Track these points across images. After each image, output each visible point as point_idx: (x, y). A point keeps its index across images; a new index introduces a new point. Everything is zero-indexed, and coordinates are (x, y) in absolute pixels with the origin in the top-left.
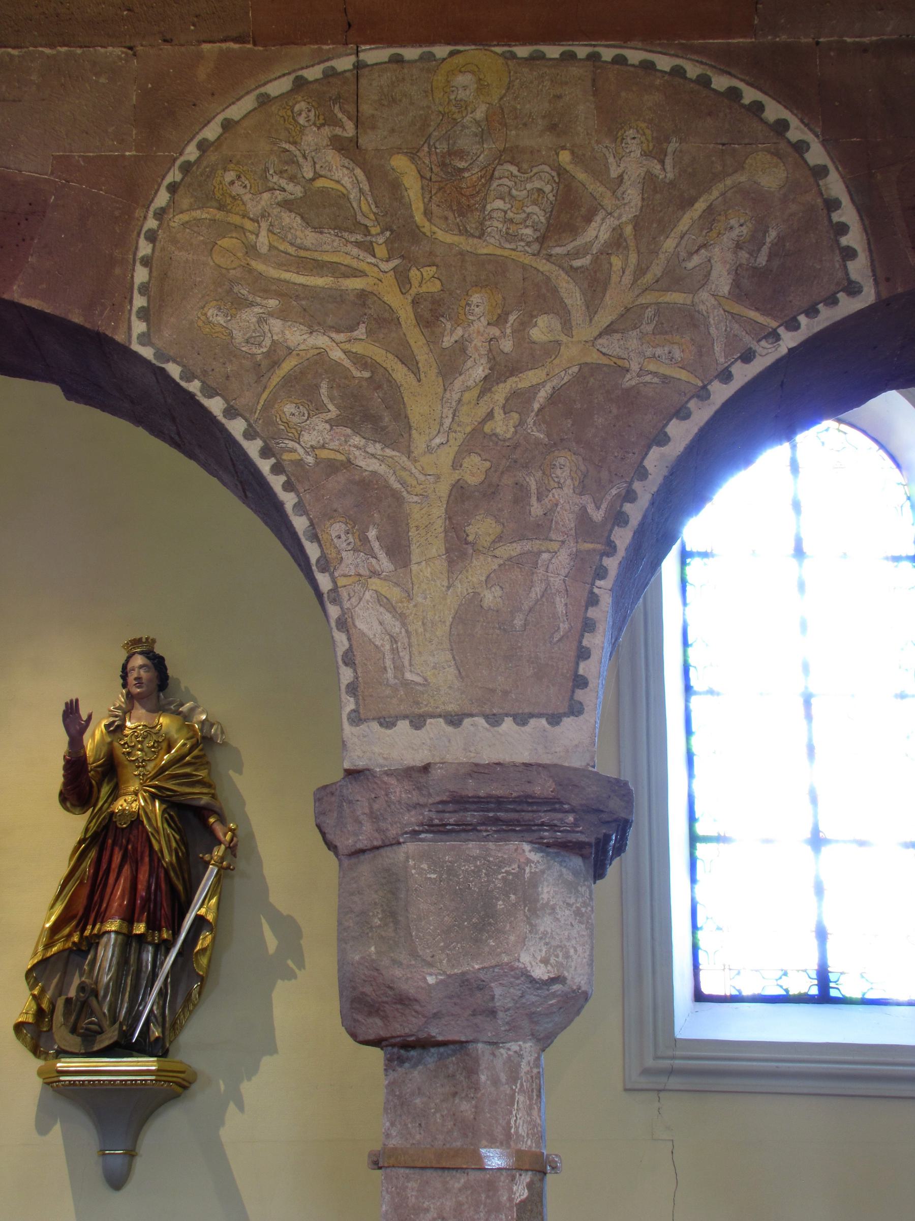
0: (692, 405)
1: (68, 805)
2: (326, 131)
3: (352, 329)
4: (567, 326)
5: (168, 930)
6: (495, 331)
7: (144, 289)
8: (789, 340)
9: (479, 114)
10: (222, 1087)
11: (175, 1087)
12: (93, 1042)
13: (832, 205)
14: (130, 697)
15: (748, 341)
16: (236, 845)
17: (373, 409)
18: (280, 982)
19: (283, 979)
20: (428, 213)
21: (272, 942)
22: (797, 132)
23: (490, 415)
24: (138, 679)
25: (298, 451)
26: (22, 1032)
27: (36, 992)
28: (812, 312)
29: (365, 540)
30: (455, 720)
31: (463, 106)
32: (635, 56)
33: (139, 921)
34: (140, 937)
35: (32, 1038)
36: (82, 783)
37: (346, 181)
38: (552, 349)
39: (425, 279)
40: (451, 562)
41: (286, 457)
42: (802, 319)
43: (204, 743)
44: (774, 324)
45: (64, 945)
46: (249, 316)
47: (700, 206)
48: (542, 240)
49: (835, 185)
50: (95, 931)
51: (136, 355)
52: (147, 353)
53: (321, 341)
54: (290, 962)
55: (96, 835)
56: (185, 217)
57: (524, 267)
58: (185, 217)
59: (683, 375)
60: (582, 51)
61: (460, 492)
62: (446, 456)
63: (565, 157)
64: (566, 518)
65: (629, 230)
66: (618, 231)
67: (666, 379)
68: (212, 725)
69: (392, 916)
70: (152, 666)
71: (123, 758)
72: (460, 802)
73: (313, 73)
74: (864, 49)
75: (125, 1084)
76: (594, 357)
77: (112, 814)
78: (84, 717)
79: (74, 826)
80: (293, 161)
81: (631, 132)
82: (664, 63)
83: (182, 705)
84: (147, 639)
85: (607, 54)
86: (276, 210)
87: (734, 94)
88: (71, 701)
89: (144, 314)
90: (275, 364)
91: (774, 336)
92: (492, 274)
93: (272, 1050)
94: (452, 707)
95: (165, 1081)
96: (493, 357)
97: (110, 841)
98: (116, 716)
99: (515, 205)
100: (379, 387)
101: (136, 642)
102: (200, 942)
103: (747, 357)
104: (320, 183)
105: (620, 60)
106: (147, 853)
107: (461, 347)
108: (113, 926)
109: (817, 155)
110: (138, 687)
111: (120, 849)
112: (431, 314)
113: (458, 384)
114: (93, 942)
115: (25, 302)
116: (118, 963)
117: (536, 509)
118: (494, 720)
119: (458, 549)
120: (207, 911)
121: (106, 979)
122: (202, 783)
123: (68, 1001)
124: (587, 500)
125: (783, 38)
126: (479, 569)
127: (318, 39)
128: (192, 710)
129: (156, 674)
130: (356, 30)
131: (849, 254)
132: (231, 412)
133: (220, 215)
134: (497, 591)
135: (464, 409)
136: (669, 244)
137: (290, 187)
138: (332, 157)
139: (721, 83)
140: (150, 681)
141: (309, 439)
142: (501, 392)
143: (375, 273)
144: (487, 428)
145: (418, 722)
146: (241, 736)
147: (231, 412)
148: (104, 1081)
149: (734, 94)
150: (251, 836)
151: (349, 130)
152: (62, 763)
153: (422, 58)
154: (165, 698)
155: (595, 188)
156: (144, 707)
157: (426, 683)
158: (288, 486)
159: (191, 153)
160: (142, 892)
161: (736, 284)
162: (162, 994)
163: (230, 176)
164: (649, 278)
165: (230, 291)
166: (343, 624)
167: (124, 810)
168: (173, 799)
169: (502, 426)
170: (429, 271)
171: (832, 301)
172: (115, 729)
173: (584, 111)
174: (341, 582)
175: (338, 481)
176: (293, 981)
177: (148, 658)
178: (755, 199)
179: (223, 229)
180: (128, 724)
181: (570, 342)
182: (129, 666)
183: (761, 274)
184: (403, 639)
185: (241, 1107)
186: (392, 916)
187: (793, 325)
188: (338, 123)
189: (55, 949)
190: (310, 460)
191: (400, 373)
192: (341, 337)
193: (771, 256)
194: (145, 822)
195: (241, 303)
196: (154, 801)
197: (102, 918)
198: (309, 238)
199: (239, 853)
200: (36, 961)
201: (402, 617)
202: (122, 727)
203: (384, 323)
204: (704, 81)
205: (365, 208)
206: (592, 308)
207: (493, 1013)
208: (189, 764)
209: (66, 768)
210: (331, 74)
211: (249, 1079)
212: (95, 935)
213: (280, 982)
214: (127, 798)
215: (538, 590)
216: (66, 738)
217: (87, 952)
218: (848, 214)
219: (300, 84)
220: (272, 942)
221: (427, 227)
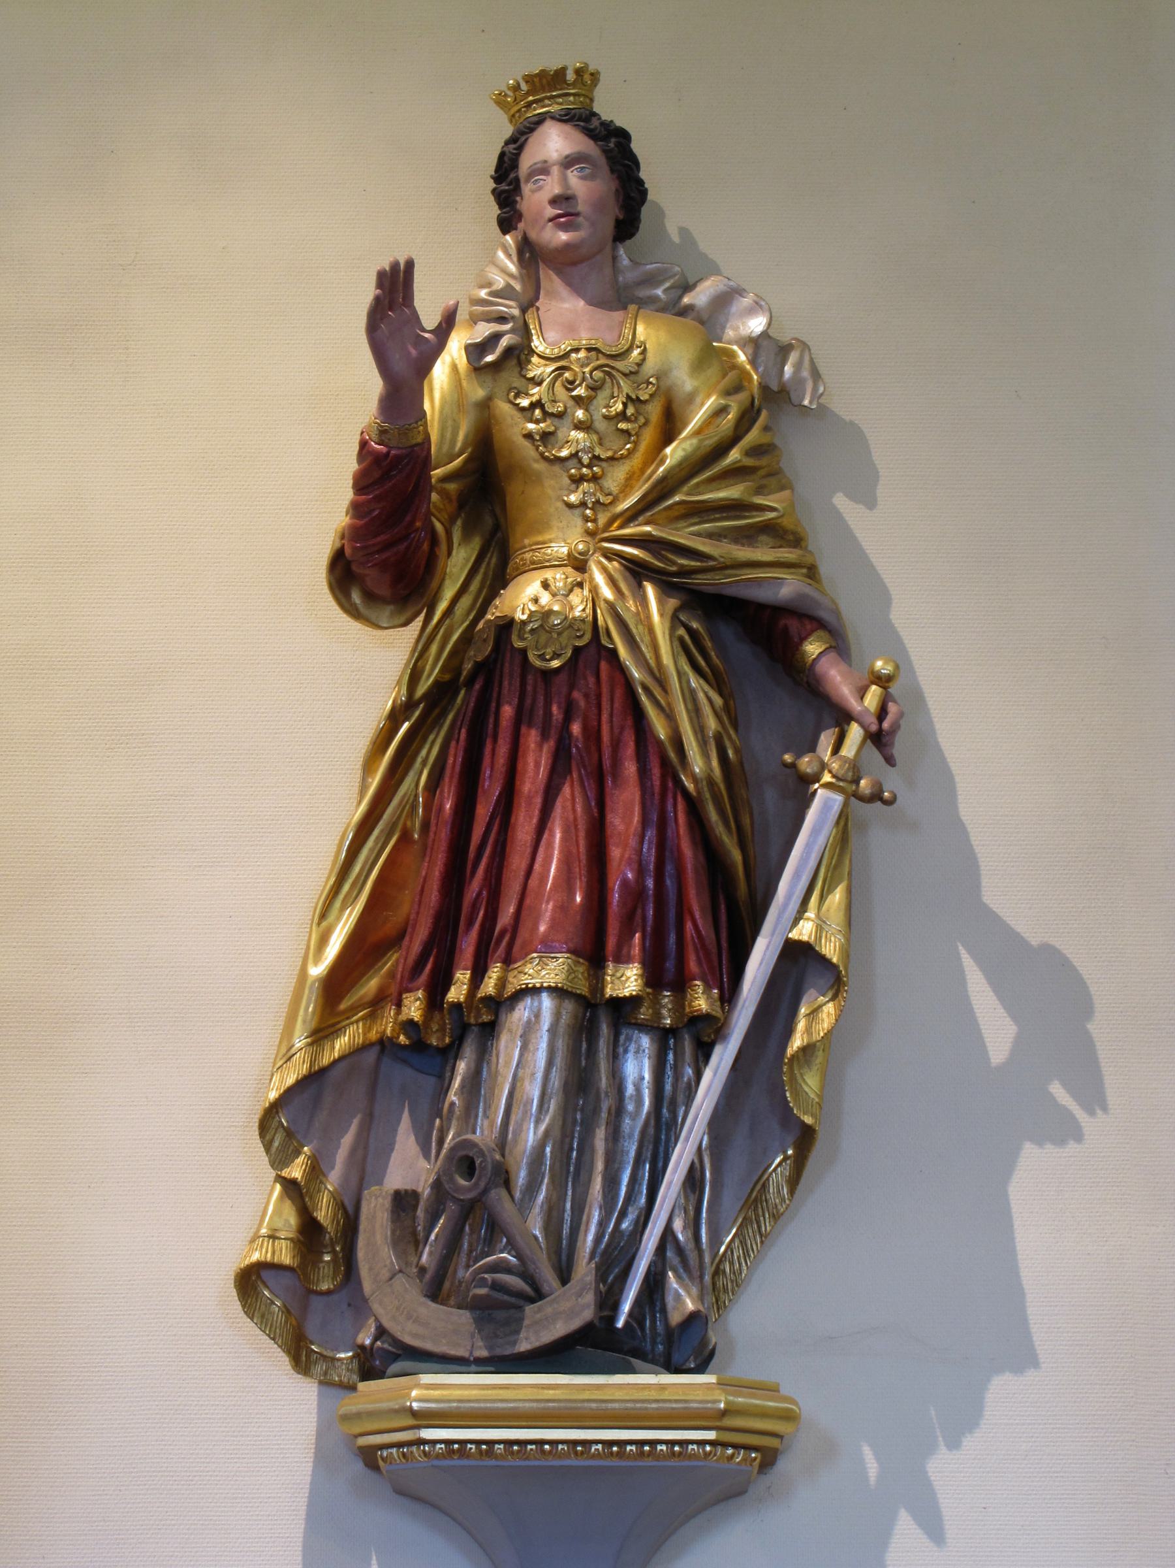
1: (356, 597)
5: (708, 987)
10: (872, 1468)
12: (514, 1326)
16: (895, 727)
18: (1030, 1153)
19: (1040, 1143)
21: (998, 1032)
24: (563, 200)
26: (258, 1295)
27: (296, 1171)
33: (622, 959)
34: (622, 1008)
35: (287, 1310)
36: (413, 524)
43: (768, 402)
45: (367, 1030)
50: (489, 986)
54: (1057, 1090)
55: (442, 693)
68: (784, 351)
70: (602, 161)
71: (528, 450)
75: (620, 1455)
77: (507, 626)
78: (430, 318)
79: (371, 665)
83: (687, 288)
84: (579, 72)
88: (395, 266)
93: (1023, 1357)
95: (735, 1446)
97: (507, 711)
98: (502, 319)
101: (547, 82)
102: (801, 1025)
106: (629, 749)
110: (565, 227)
111: (544, 736)
114: (482, 1023)
116: (566, 1086)
120: (819, 929)
121: (531, 1136)
122: (775, 532)
123: (403, 1201)
128: (723, 301)
129: (613, 185)
140: (599, 206)
146: (859, 388)
148: (554, 1443)
150: (918, 697)
152: (350, 465)
154: (635, 263)
156: (578, 290)
160: (622, 869)
162: (693, 1181)
167: (548, 613)
168: (699, 580)
172: (503, 361)
176: (1072, 1147)
177: (591, 134)
180: (538, 344)
182: (526, 162)
189: (341, 1044)
194: (623, 652)
196: (640, 586)
197: (500, 945)
199: (899, 748)
200: (291, 1080)
202: (519, 354)
208: (736, 473)
209: (362, 484)
211: (954, 1444)
212: (488, 999)
213: (1030, 1153)
214: (548, 574)
216: (373, 385)
217: (450, 1053)
220: (998, 1032)
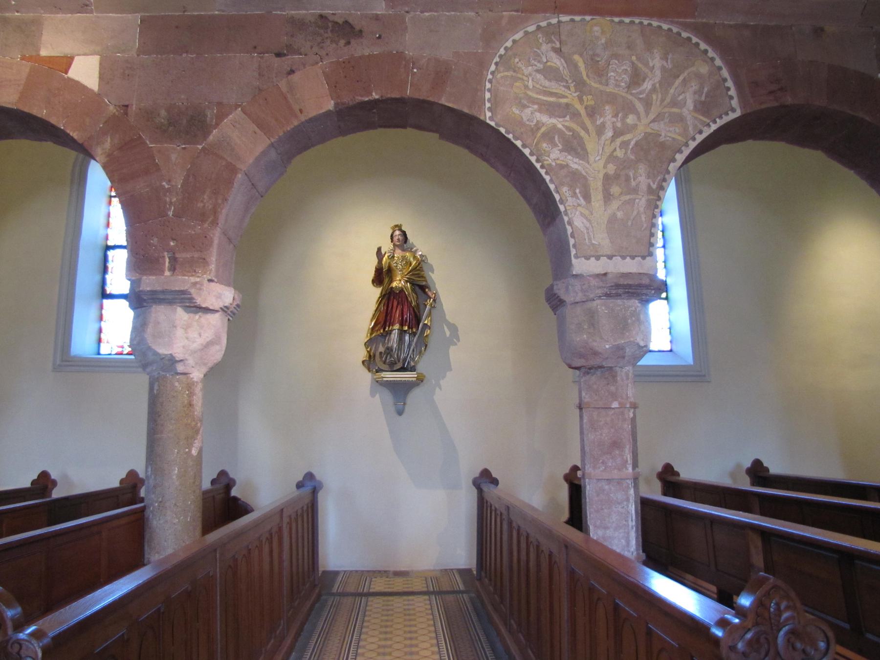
0: (683, 148)
2: (550, 45)
3: (565, 117)
4: (639, 118)
6: (615, 120)
7: (489, 100)
8: (714, 127)
9: (603, 41)
11: (420, 380)
13: (725, 80)
14: (394, 245)
15: (700, 126)
17: (574, 146)
20: (587, 76)
21: (448, 333)
22: (711, 54)
23: (615, 150)
25: (549, 161)
28: (720, 117)
29: (575, 193)
30: (610, 257)
31: (597, 38)
32: (655, 23)
36: (381, 276)
37: (558, 63)
38: (635, 126)
39: (589, 100)
40: (605, 202)
41: (545, 162)
42: (718, 120)
44: (708, 121)
46: (528, 111)
47: (681, 78)
48: (628, 87)
49: (725, 73)
51: (488, 125)
52: (492, 124)
53: (554, 121)
55: (385, 295)
56: (502, 74)
57: (623, 97)
58: (502, 74)
59: (679, 138)
60: (637, 21)
61: (607, 177)
62: (601, 164)
63: (634, 58)
64: (643, 187)
65: (658, 85)
66: (654, 85)
67: (674, 139)
69: (592, 325)
72: (618, 286)
73: (543, 24)
74: (731, 26)
76: (649, 130)
79: (377, 292)
80: (539, 55)
81: (655, 51)
82: (665, 27)
85: (646, 22)
86: (534, 73)
87: (689, 39)
89: (490, 109)
90: (539, 129)
91: (708, 125)
92: (612, 99)
94: (609, 253)
96: (614, 128)
99: (618, 75)
100: (575, 138)
101: (396, 226)
103: (701, 132)
104: (549, 64)
105: (650, 25)
107: (603, 125)
108: (397, 326)
109: (718, 62)
112: (592, 113)
113: (603, 138)
114: (390, 332)
115: (447, 104)
117: (633, 183)
118: (623, 257)
119: (608, 197)
123: (381, 353)
124: (650, 181)
125: (704, 20)
126: (615, 204)
127: (545, 11)
130: (559, 9)
131: (731, 98)
132: (524, 146)
133: (514, 74)
134: (622, 212)
135: (606, 148)
136: (672, 91)
137: (538, 65)
138: (553, 55)
139: (685, 35)
141: (553, 156)
142: (618, 141)
143: (571, 97)
144: (615, 154)
145: (598, 258)
147: (524, 146)
149: (689, 39)
151: (558, 45)
153: (581, 20)
155: (644, 69)
157: (599, 245)
158: (547, 173)
159: (502, 51)
161: (695, 106)
163: (517, 60)
164: (665, 103)
165: (520, 102)
166: (570, 223)
169: (619, 153)
170: (590, 97)
171: (727, 114)
173: (639, 42)
174: (568, 208)
175: (563, 172)
178: (699, 76)
179: (517, 79)
181: (641, 124)
183: (703, 103)
184: (591, 229)
185: (440, 388)
186: (592, 325)
187: (715, 122)
188: (554, 42)
190: (554, 164)
191: (583, 133)
192: (561, 120)
193: (706, 97)
195: (525, 107)
198: (547, 83)
201: (589, 221)
202: (393, 257)
203: (575, 115)
204: (679, 34)
205: (565, 73)
206: (647, 113)
207: (624, 357)
210: (549, 24)
215: (635, 213)
218: (730, 83)
219: (539, 28)
220: (448, 333)
221: (588, 81)
